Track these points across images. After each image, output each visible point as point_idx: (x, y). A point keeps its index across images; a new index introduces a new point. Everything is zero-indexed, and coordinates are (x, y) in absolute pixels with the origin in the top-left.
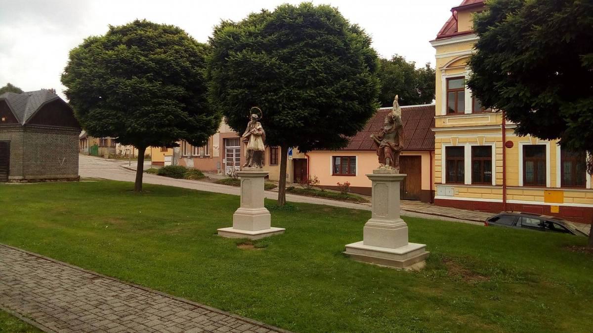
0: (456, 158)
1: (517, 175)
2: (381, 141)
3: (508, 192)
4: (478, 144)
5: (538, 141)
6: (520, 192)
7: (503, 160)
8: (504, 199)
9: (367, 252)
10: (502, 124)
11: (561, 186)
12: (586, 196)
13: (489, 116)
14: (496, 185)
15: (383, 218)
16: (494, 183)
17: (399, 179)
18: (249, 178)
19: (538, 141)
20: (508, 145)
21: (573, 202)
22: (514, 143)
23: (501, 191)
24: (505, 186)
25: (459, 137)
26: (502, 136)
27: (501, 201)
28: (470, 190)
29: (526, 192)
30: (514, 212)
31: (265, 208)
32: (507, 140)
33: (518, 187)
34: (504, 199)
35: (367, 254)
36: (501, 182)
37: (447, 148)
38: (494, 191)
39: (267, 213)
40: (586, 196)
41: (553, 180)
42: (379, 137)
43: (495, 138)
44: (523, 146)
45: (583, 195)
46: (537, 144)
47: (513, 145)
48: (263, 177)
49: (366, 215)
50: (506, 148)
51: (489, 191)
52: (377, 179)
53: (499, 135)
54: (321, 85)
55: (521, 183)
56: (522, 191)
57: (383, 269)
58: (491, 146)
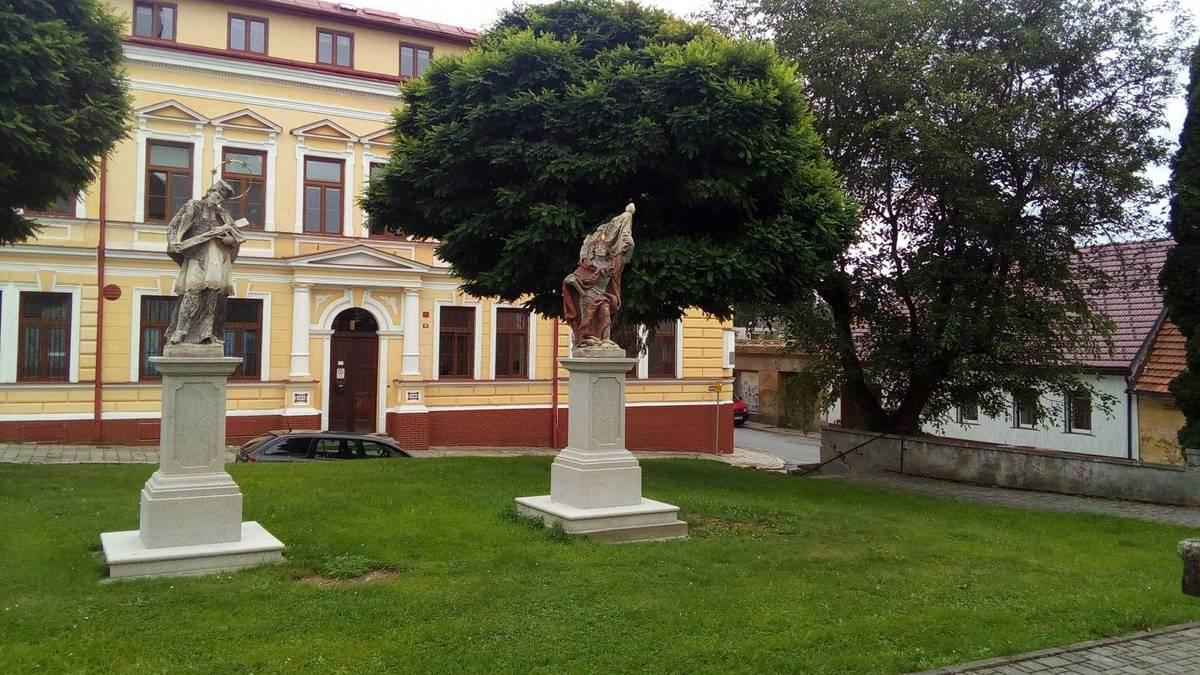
0: (457, 330)
1: (125, 359)
2: (584, 289)
3: (106, 395)
4: (39, 288)
5: (467, 300)
6: (133, 394)
7: (98, 326)
8: (98, 410)
9: (615, 521)
10: (99, 247)
11: (496, 377)
12: (68, 396)
13: (69, 227)
14: (81, 382)
15: (610, 448)
16: (74, 377)
17: (622, 368)
18: (207, 379)
19: (467, 300)
20: (110, 293)
21: (43, 412)
22: (121, 289)
23: (91, 395)
24: (98, 384)
25: (59, 270)
26: (95, 273)
27: (91, 416)
28: (649, 389)
29: (500, 390)
30: (293, 431)
31: (626, 452)
32: (107, 283)
33: (129, 383)
34: (98, 410)
35: (615, 526)
36: (91, 375)
37: (144, 298)
38: (74, 395)
39: (230, 490)
40: (68, 396)
41: (485, 367)
42: (585, 283)
43: (10, 274)
44: (23, 294)
45: (255, 393)
46: (246, 297)
47: (119, 295)
48: (620, 372)
49: (147, 471)
50: (105, 300)
51: (62, 395)
52: (598, 368)
53: (92, 271)
54: (778, 148)
55: (134, 376)
56: (257, 390)
57: (667, 544)
58: (71, 294)
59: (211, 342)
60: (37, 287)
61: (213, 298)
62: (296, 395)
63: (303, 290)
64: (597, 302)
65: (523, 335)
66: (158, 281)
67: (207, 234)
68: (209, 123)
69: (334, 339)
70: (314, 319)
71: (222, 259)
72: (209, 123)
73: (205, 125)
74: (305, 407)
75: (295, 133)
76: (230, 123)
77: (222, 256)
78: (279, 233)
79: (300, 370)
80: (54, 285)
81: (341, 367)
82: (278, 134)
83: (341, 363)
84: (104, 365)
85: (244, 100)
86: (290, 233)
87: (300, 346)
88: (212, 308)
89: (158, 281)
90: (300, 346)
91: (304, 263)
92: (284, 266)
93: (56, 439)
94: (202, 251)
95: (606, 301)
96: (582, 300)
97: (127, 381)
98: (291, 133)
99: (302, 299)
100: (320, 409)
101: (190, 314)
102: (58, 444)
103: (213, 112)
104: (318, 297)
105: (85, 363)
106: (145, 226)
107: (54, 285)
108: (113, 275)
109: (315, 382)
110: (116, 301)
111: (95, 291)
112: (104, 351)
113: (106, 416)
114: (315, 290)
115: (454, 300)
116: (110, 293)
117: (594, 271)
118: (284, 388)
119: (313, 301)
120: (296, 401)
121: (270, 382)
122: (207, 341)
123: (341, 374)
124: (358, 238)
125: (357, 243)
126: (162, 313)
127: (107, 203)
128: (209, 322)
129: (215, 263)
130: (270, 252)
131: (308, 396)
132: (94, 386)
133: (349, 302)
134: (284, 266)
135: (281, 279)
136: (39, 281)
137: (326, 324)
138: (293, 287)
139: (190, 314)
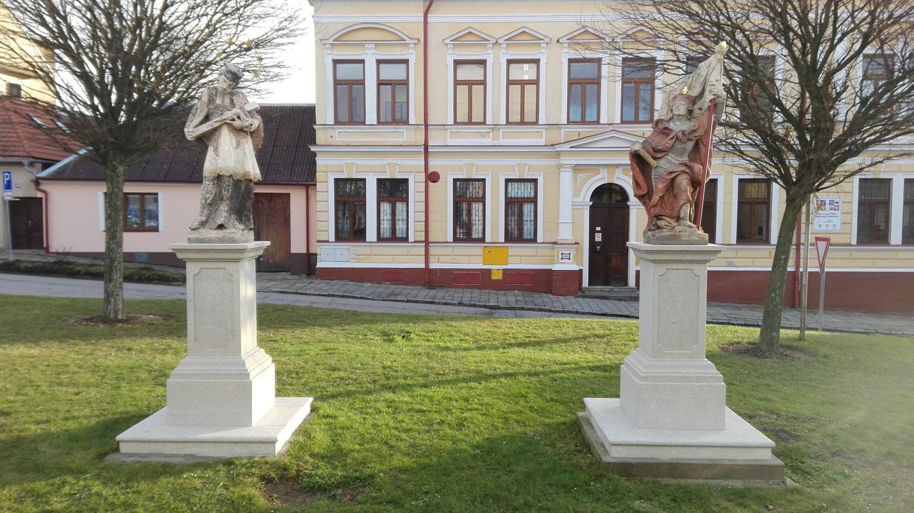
2: (655, 158)
10: (424, 145)
11: (737, 242)
13: (405, 131)
14: (415, 242)
18: (221, 265)
20: (432, 177)
25: (357, 162)
27: (423, 266)
28: (901, 255)
29: (741, 254)
32: (430, 170)
33: (447, 242)
34: (427, 262)
37: (455, 180)
42: (655, 151)
50: (429, 182)
59: (225, 228)
60: (344, 175)
61: (226, 183)
62: (562, 254)
63: (566, 170)
64: (671, 173)
65: (765, 203)
66: (464, 167)
67: (217, 119)
68: (497, 42)
69: (593, 209)
70: (576, 194)
71: (235, 145)
72: (497, 42)
73: (494, 44)
74: (568, 263)
75: (561, 41)
76: (511, 40)
77: (234, 141)
78: (549, 125)
79: (565, 234)
80: (397, 173)
81: (598, 232)
82: (548, 43)
83: (598, 229)
84: (430, 229)
85: (523, 19)
86: (557, 125)
87: (566, 214)
88: (226, 194)
89: (344, 166)
90: (566, 214)
91: (566, 148)
92: (552, 150)
93: (399, 281)
94: (215, 137)
95: (684, 172)
96: (653, 172)
97: (445, 241)
98: (558, 41)
99: (566, 177)
100: (582, 265)
101: (206, 200)
102: (403, 284)
103: (499, 33)
104: (580, 175)
105: (418, 228)
106: (454, 127)
107: (397, 173)
108: (435, 164)
109: (577, 243)
110: (437, 183)
111: (422, 177)
112: (430, 219)
113: (432, 266)
114: (577, 168)
115: (517, 173)
116: (432, 177)
117: (668, 135)
118: (554, 248)
119: (575, 179)
120: (562, 259)
121: (543, 243)
122: (221, 227)
123: (598, 238)
124: (611, 124)
125: (611, 128)
126: (516, 191)
127: (428, 113)
128: (224, 208)
129: (227, 149)
130: (542, 141)
131: (571, 255)
132: (424, 244)
133: (604, 178)
134: (552, 150)
135: (552, 162)
136: (387, 170)
137: (585, 199)
138: (559, 167)
139: (206, 200)
